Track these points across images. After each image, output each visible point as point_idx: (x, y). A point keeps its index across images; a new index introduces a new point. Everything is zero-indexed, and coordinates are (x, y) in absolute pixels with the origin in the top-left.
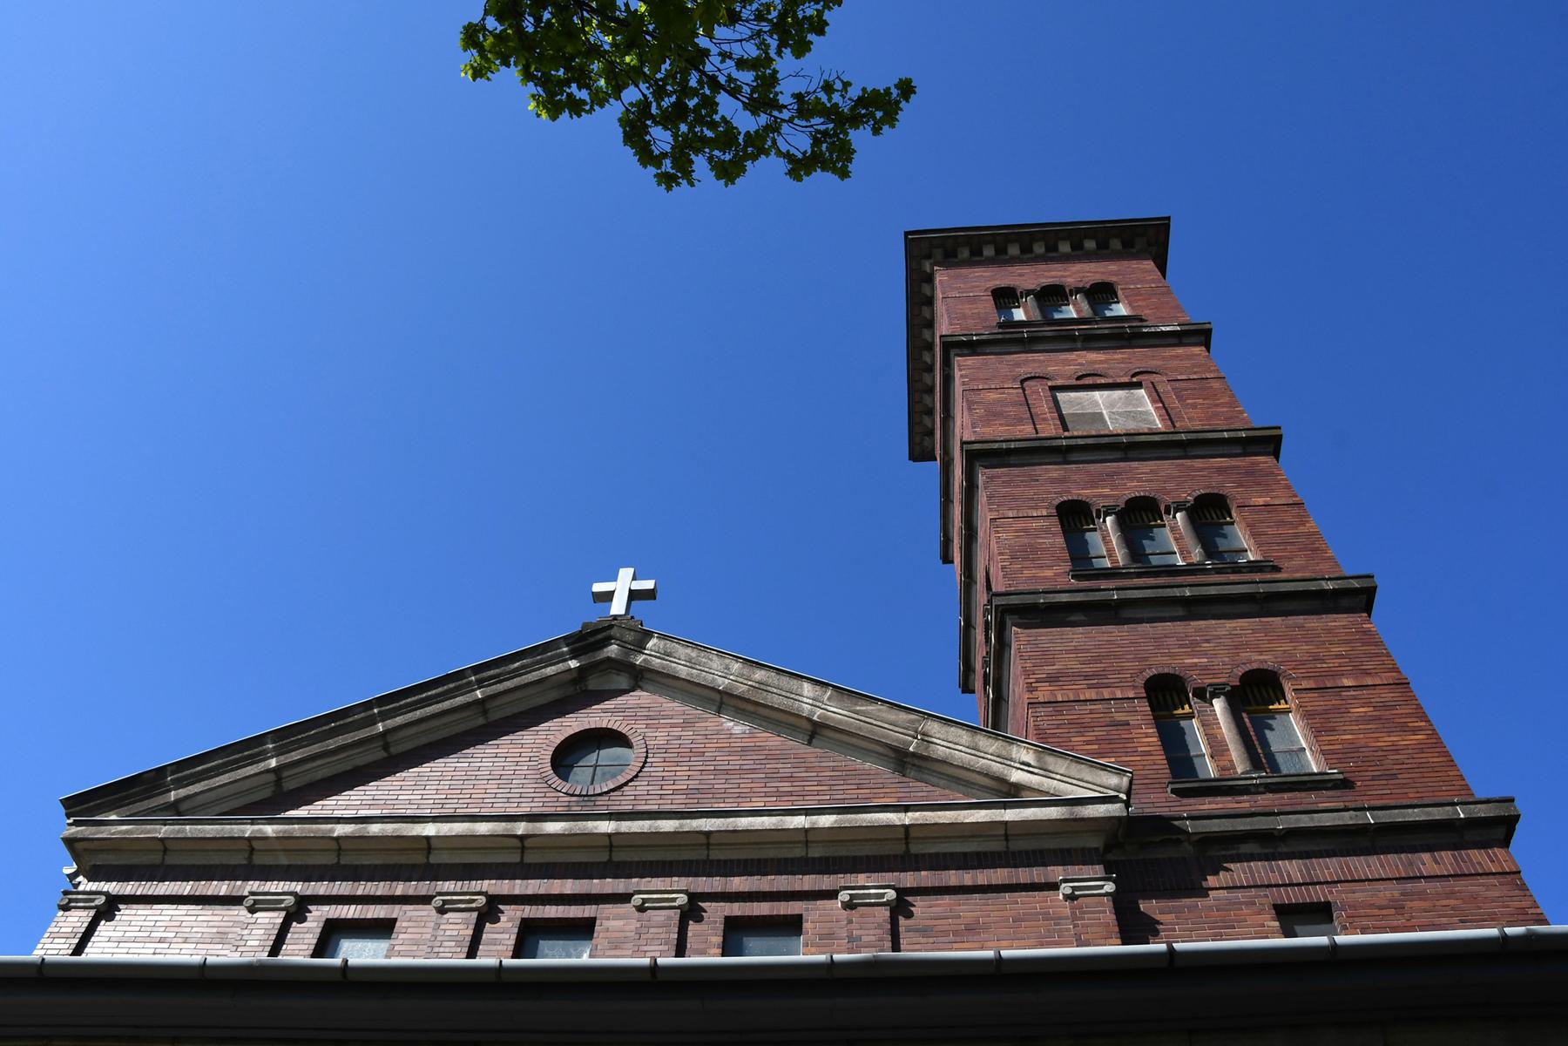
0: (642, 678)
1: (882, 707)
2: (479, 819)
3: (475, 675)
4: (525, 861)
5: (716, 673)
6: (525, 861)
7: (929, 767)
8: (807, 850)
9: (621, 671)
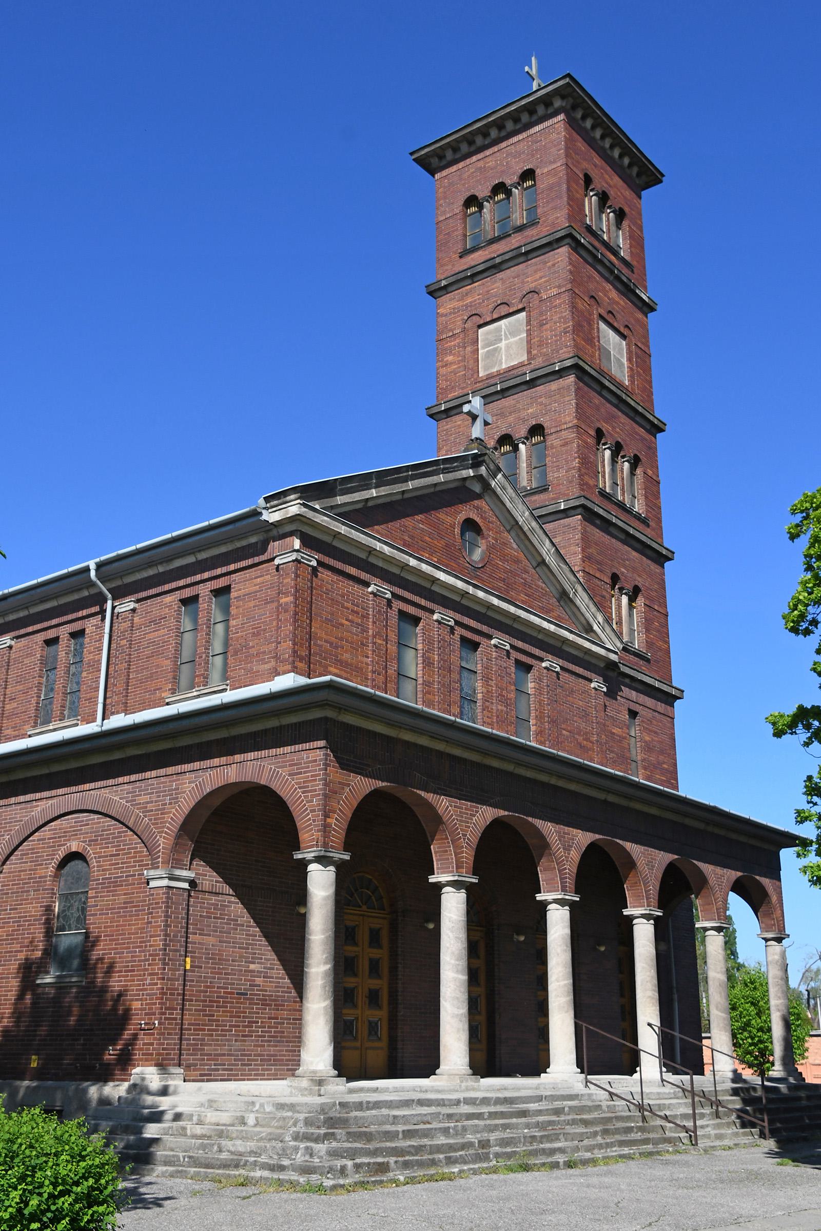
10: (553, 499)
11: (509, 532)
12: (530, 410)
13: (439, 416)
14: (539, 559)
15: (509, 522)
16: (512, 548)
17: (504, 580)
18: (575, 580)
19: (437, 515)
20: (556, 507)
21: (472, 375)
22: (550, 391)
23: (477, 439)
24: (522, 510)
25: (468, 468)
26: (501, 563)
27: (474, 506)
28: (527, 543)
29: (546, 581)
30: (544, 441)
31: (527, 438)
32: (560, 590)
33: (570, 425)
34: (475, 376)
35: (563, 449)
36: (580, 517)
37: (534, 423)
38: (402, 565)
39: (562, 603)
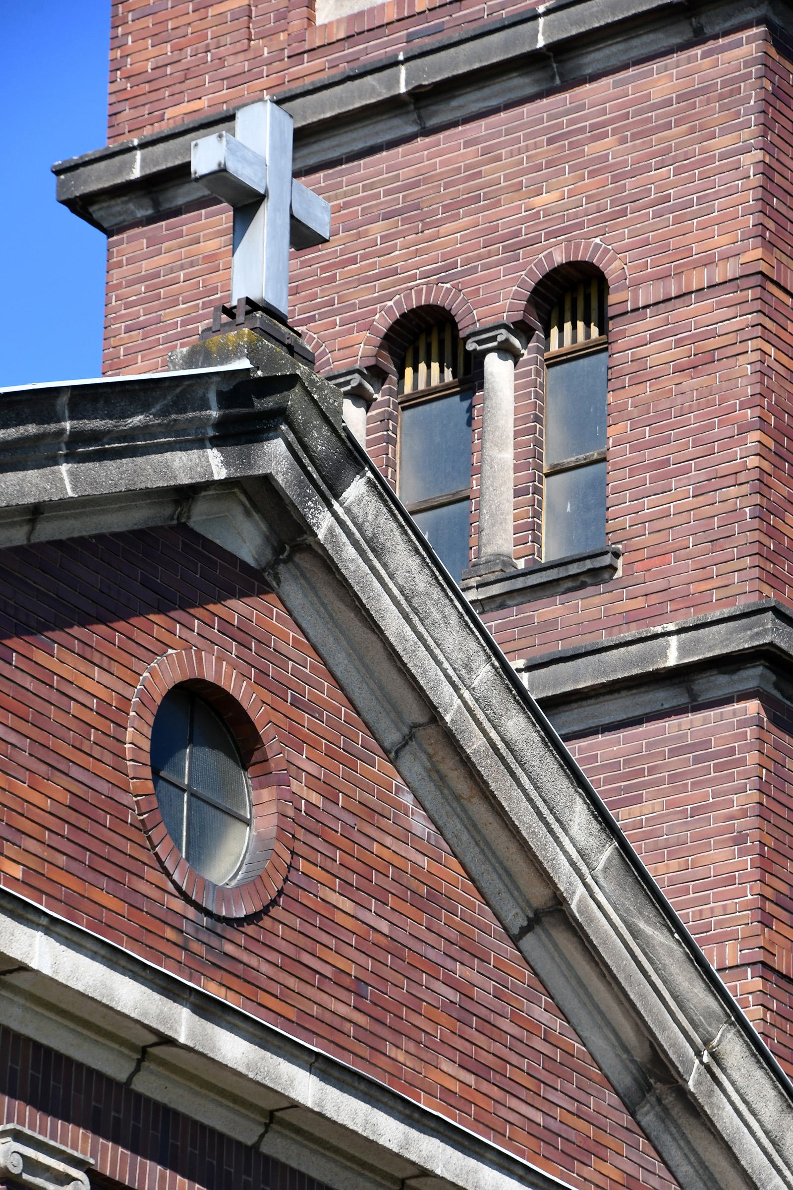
0: (289, 559)
1: (675, 946)
2: (123, 962)
3: (72, 418)
4: (133, 1086)
5: (446, 665)
6: (133, 1086)
7: (680, 1121)
8: (137, 1070)
9: (258, 511)
10: (631, 618)
11: (393, 755)
12: (545, 198)
13: (119, 209)
14: (539, 895)
15: (394, 709)
16: (406, 836)
17: (357, 987)
18: (711, 1003)
19: (40, 656)
20: (643, 659)
21: (282, 16)
22: (644, 105)
23: (252, 305)
24: (458, 657)
25: (200, 444)
26: (348, 906)
27: (226, 628)
28: (480, 810)
29: (571, 1003)
30: (602, 348)
31: (523, 330)
32: (641, 1053)
33: (731, 269)
34: (296, 23)
35: (690, 383)
36: (753, 706)
37: (559, 258)
38: (269, 1105)
39: (648, 1118)
